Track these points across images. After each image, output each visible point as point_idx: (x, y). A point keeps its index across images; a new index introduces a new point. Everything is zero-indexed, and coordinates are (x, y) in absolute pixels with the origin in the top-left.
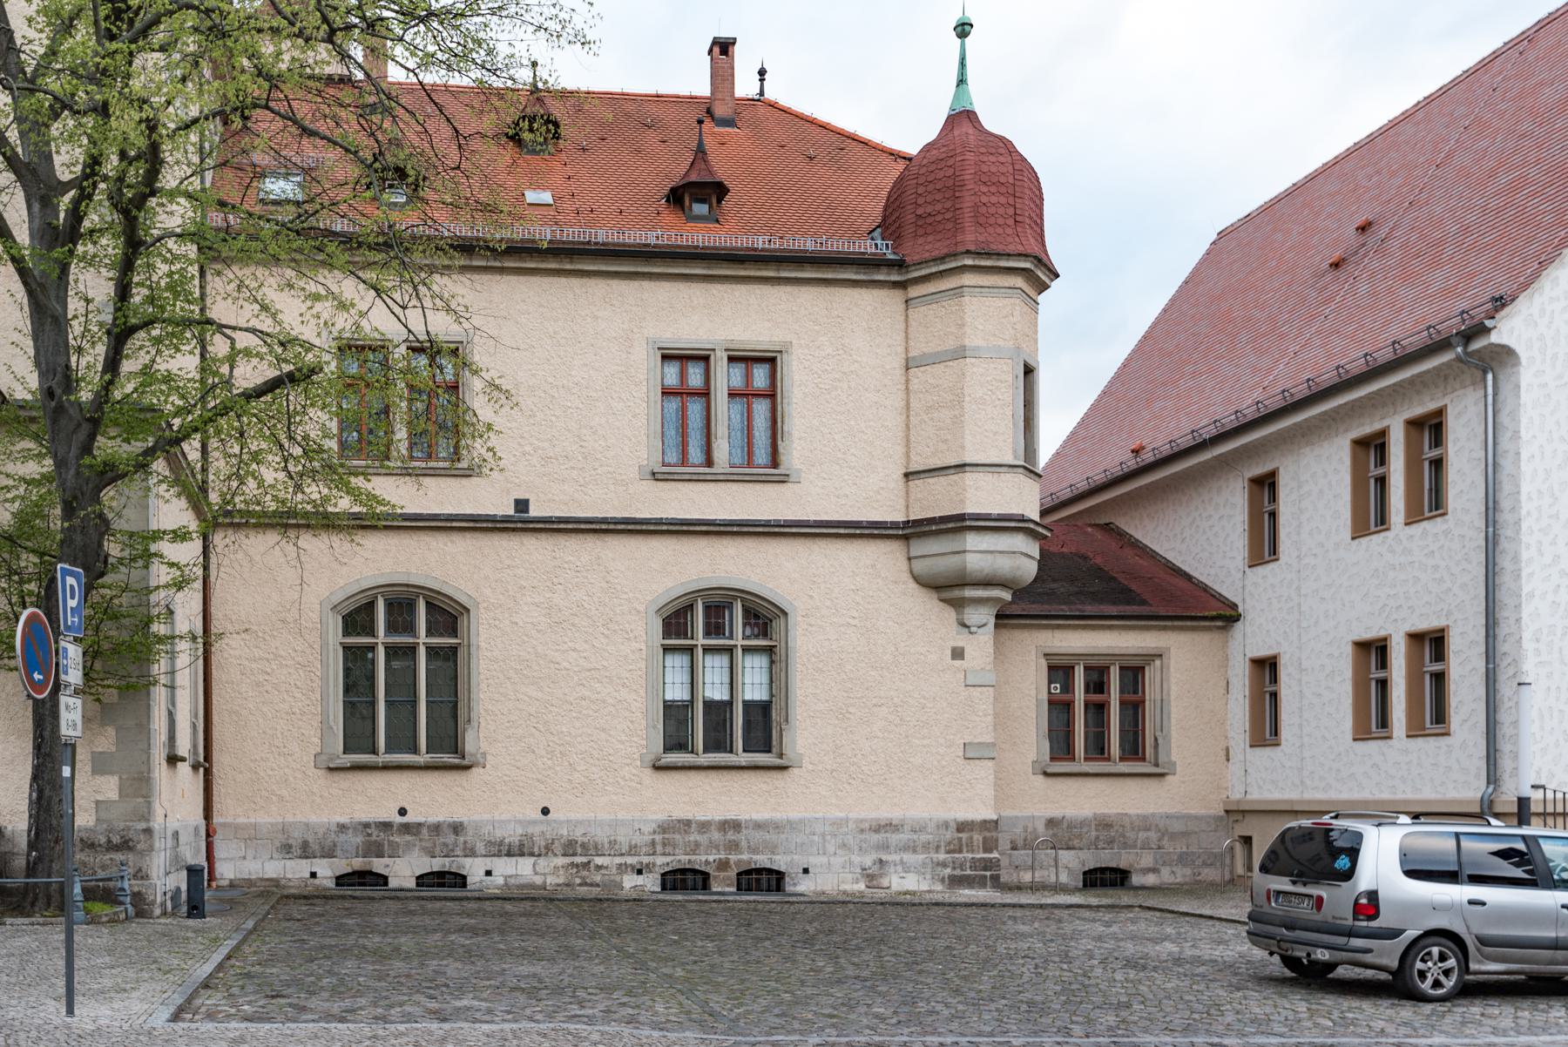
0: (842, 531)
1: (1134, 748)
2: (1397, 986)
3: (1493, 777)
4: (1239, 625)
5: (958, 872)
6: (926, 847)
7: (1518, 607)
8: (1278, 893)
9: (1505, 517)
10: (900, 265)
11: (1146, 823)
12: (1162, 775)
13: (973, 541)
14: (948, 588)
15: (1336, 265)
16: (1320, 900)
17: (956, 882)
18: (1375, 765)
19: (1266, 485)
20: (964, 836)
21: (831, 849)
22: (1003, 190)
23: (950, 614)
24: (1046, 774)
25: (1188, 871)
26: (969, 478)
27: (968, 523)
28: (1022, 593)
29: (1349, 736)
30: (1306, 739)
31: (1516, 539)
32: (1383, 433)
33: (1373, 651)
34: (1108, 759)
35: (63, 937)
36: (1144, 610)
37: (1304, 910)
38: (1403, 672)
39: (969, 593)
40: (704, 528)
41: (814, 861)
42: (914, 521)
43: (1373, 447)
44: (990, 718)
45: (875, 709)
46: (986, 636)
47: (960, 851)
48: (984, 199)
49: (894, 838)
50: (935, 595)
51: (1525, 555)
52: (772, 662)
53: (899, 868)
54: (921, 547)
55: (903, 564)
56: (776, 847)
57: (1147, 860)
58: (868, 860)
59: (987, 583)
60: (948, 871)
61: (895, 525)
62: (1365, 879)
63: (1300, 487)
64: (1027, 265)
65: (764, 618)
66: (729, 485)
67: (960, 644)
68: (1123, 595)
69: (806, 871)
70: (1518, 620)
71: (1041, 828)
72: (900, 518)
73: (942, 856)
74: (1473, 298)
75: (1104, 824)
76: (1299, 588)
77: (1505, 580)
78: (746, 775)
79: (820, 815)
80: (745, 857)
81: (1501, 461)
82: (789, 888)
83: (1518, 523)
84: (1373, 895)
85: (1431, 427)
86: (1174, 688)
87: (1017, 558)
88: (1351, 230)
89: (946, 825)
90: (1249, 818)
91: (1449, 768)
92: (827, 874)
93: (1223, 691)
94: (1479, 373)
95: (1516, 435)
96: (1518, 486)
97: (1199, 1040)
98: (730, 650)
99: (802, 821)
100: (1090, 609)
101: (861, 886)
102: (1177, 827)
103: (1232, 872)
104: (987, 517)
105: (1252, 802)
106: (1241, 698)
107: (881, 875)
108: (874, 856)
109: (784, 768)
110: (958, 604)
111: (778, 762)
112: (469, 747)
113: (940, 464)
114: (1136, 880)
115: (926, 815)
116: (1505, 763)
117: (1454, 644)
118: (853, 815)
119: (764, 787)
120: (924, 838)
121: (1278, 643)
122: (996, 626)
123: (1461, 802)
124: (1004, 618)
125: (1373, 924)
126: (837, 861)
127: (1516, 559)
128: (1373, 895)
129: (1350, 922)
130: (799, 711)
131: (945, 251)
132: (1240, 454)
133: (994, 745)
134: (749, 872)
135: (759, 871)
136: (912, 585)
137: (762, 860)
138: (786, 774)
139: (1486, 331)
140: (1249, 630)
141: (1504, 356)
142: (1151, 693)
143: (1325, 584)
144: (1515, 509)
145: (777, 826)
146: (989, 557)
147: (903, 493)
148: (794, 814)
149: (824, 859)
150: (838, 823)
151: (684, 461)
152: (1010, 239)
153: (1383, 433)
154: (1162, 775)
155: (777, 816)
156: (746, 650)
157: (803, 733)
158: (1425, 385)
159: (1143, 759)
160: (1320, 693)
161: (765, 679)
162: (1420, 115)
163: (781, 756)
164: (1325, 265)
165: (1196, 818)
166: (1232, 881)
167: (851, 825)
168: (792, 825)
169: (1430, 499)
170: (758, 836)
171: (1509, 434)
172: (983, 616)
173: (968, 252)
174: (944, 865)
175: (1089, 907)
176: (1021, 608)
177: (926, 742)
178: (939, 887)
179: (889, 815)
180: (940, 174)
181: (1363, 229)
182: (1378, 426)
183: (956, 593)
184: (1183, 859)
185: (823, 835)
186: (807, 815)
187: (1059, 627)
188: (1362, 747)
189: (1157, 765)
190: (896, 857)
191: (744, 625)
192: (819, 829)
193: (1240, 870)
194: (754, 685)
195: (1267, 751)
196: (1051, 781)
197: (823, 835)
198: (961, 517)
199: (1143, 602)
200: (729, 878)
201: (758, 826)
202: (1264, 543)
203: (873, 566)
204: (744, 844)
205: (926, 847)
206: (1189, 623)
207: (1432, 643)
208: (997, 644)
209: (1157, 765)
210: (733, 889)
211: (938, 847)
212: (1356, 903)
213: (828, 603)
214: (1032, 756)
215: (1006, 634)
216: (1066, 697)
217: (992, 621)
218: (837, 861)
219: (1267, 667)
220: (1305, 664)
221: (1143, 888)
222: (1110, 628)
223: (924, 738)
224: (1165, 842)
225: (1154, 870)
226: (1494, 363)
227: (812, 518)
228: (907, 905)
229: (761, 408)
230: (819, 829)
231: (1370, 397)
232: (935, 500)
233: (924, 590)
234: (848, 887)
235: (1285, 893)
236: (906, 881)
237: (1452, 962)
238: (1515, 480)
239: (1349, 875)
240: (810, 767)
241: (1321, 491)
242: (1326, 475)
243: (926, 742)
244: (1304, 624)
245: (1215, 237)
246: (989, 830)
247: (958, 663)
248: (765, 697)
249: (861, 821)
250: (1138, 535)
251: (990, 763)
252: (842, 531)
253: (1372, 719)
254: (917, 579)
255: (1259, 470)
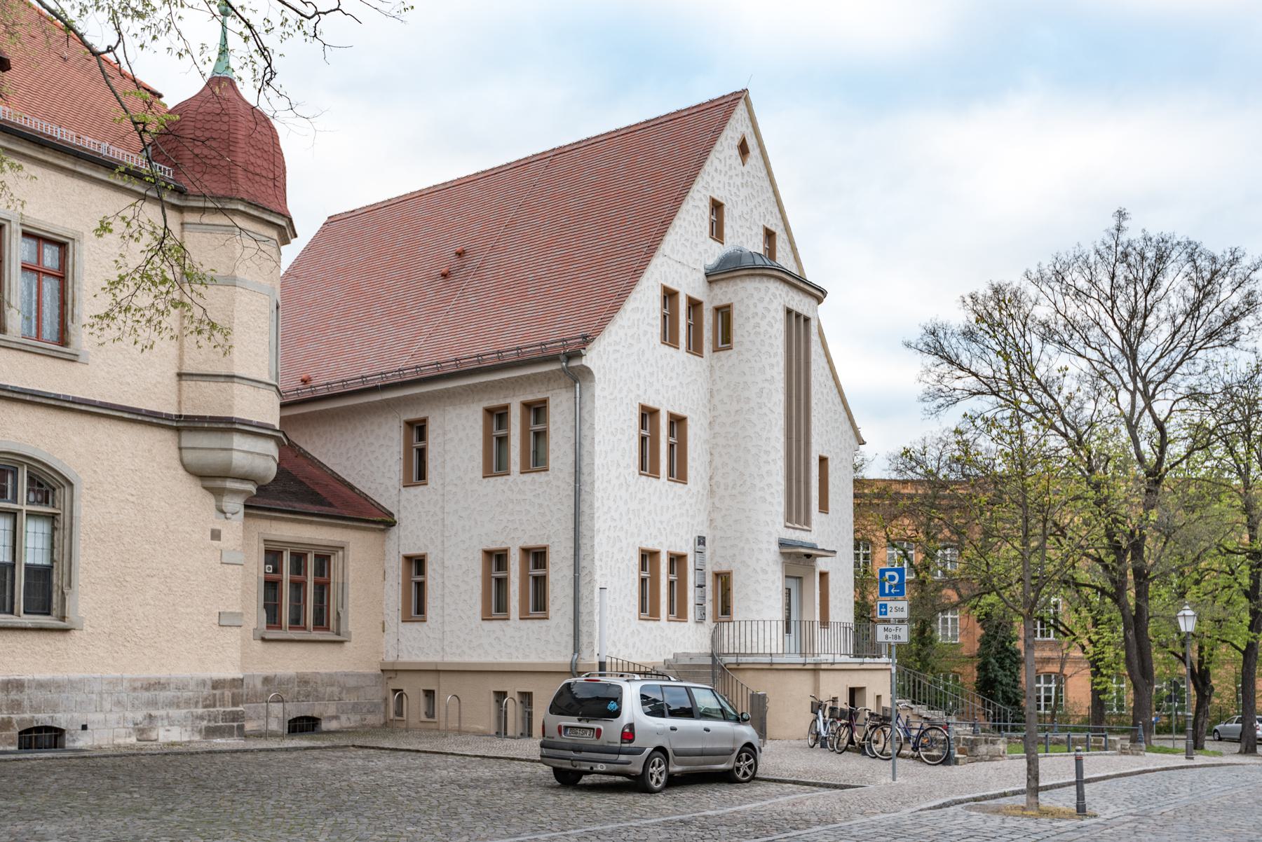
0: (126, 415)
1: (321, 621)
2: (638, 784)
3: (576, 649)
4: (395, 529)
5: (212, 724)
6: (187, 703)
7: (592, 538)
8: (566, 727)
9: (585, 478)
10: (179, 191)
11: (331, 680)
12: (342, 642)
13: (239, 442)
14: (212, 479)
15: (444, 275)
16: (599, 731)
17: (211, 732)
18: (498, 638)
19: (418, 429)
20: (217, 692)
21: (107, 706)
22: (265, 156)
23: (210, 501)
24: (264, 640)
25: (358, 717)
26: (238, 388)
27: (237, 426)
28: (262, 489)
29: (479, 616)
30: (447, 618)
31: (591, 493)
32: (506, 407)
33: (497, 558)
34: (305, 628)
35: (1024, 763)
36: (325, 510)
37: (588, 739)
38: (518, 574)
39: (230, 484)
40: (10, 395)
41: (92, 717)
42: (186, 417)
43: (498, 416)
44: (239, 592)
45: (148, 579)
46: (238, 521)
47: (214, 706)
48: (253, 160)
49: (163, 695)
50: (199, 483)
51: (597, 505)
52: (54, 529)
53: (166, 722)
54: (190, 440)
55: (174, 453)
56: (56, 705)
57: (332, 710)
58: (139, 716)
59: (244, 478)
60: (205, 723)
61: (168, 417)
62: (625, 718)
63: (445, 434)
64: (283, 224)
65: (48, 485)
66: (21, 354)
67: (218, 527)
68: (316, 498)
69: (84, 727)
70: (592, 546)
71: (259, 685)
72: (174, 412)
73: (200, 711)
74: (572, 331)
75: (303, 681)
76: (443, 508)
77: (584, 518)
78: (30, 636)
79: (97, 675)
80: (27, 716)
81: (583, 442)
82: (68, 745)
83: (593, 483)
84: (631, 726)
85: (537, 410)
86: (351, 574)
87: (257, 457)
88: (452, 255)
89: (204, 683)
90: (400, 675)
91: (547, 642)
92: (103, 730)
93: (381, 578)
94: (570, 381)
95: (592, 427)
96: (593, 459)
97: (541, 837)
98: (14, 514)
99: (81, 681)
100: (299, 506)
101: (133, 740)
102: (352, 682)
103: (385, 717)
104: (249, 423)
105: (404, 663)
106: (395, 584)
107: (150, 729)
108: (145, 712)
109: (65, 630)
110: (218, 493)
111: (61, 624)
112: (69, 613)
113: (211, 371)
114: (325, 726)
115: (187, 675)
116: (584, 639)
117: (552, 557)
118: (127, 675)
119: (47, 648)
120: (187, 694)
121: (426, 546)
122: (246, 515)
123: (556, 664)
124: (251, 507)
125: (632, 745)
126: (113, 717)
127: (591, 506)
128: (631, 726)
129: (618, 745)
130: (81, 576)
131: (222, 192)
132: (403, 400)
133: (242, 614)
134: (28, 731)
135: (39, 729)
136: (181, 472)
137: (43, 718)
138: (67, 635)
139: (580, 355)
140: (402, 533)
141: (586, 373)
142: (335, 577)
143: (461, 508)
144: (591, 474)
145: (57, 686)
146: (250, 456)
147: (175, 389)
148: (75, 675)
149: (100, 716)
150: (114, 682)
151: (38, 337)
152: (271, 199)
153: (506, 407)
154: (342, 642)
155: (59, 676)
156: (30, 515)
157: (85, 598)
158: (535, 381)
159: (328, 629)
160: (457, 585)
161: (46, 545)
162: (482, 183)
163: (63, 618)
164: (436, 273)
165: (364, 675)
166: (385, 724)
167: (126, 684)
168: (72, 684)
169: (536, 460)
170: (40, 695)
171: (588, 425)
172: (235, 505)
173: (242, 200)
174: (201, 718)
175: (319, 748)
176: (267, 499)
177: (189, 610)
178: (197, 738)
179: (158, 675)
180: (216, 126)
181: (460, 254)
182: (502, 402)
183: (218, 483)
184: (355, 708)
185: (101, 693)
186: (86, 675)
187: (275, 518)
188: (487, 624)
189: (338, 634)
190: (162, 712)
191: (28, 491)
192: (97, 688)
193: (392, 715)
194: (35, 549)
195: (416, 625)
196: (267, 645)
197: (101, 693)
198: (230, 420)
199: (331, 505)
200: (11, 737)
201: (41, 685)
202: (418, 469)
203: (150, 451)
204: (26, 703)
205: (187, 703)
206: (363, 525)
207: (537, 556)
208: (245, 528)
209: (338, 634)
210: (15, 748)
211: (197, 702)
212: (623, 732)
213: (110, 479)
214: (253, 625)
215: (251, 522)
216: (276, 576)
217: (242, 510)
218: (113, 717)
219: (417, 564)
220: (447, 564)
221: (329, 732)
222: (311, 523)
223: (188, 606)
224: (344, 695)
225: (336, 718)
226: (579, 377)
227: (98, 399)
228: (173, 754)
229: (49, 286)
230: (97, 688)
231: (500, 381)
232: (205, 400)
233: (191, 477)
234: (121, 741)
235: (572, 727)
236: (171, 734)
237: (663, 767)
238: (591, 454)
239: (617, 714)
240: (90, 630)
241: (461, 440)
242: (464, 429)
243: (189, 610)
244: (447, 534)
245: (325, 219)
246: (236, 687)
247: (216, 543)
248: (46, 562)
249: (135, 680)
250: (308, 448)
251: (238, 630)
252: (126, 415)
253: (496, 605)
254: (186, 467)
255: (413, 415)
